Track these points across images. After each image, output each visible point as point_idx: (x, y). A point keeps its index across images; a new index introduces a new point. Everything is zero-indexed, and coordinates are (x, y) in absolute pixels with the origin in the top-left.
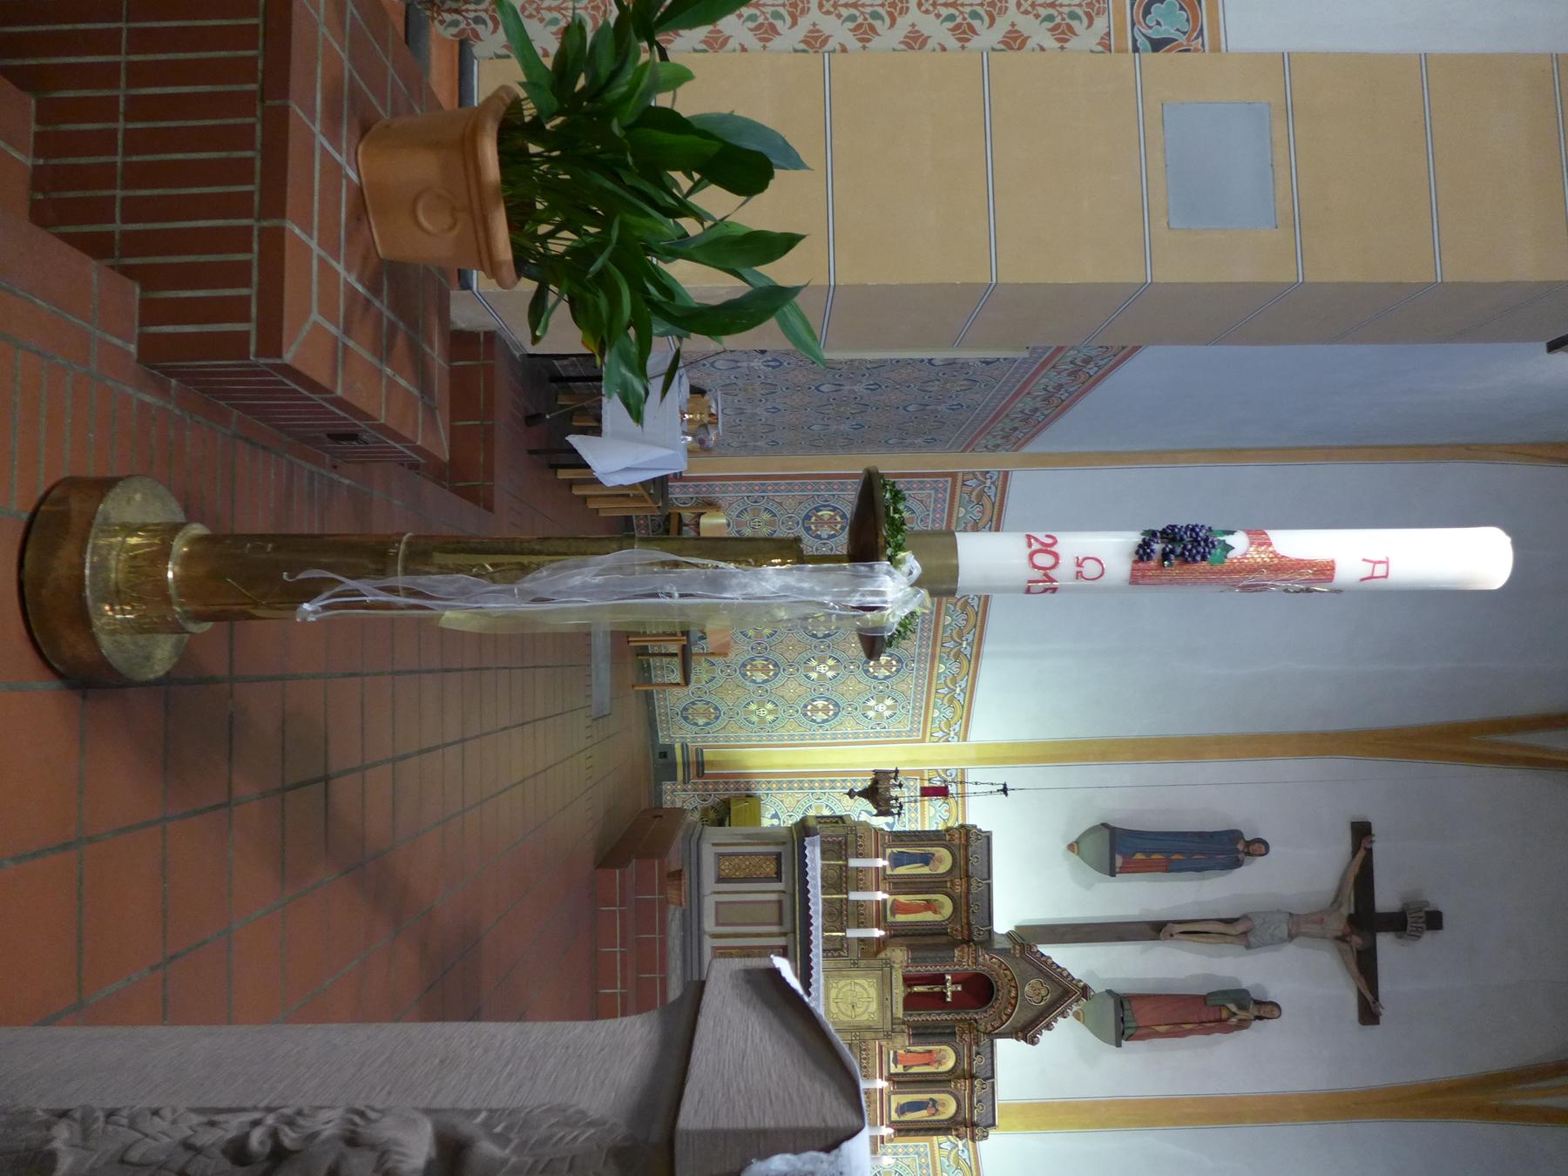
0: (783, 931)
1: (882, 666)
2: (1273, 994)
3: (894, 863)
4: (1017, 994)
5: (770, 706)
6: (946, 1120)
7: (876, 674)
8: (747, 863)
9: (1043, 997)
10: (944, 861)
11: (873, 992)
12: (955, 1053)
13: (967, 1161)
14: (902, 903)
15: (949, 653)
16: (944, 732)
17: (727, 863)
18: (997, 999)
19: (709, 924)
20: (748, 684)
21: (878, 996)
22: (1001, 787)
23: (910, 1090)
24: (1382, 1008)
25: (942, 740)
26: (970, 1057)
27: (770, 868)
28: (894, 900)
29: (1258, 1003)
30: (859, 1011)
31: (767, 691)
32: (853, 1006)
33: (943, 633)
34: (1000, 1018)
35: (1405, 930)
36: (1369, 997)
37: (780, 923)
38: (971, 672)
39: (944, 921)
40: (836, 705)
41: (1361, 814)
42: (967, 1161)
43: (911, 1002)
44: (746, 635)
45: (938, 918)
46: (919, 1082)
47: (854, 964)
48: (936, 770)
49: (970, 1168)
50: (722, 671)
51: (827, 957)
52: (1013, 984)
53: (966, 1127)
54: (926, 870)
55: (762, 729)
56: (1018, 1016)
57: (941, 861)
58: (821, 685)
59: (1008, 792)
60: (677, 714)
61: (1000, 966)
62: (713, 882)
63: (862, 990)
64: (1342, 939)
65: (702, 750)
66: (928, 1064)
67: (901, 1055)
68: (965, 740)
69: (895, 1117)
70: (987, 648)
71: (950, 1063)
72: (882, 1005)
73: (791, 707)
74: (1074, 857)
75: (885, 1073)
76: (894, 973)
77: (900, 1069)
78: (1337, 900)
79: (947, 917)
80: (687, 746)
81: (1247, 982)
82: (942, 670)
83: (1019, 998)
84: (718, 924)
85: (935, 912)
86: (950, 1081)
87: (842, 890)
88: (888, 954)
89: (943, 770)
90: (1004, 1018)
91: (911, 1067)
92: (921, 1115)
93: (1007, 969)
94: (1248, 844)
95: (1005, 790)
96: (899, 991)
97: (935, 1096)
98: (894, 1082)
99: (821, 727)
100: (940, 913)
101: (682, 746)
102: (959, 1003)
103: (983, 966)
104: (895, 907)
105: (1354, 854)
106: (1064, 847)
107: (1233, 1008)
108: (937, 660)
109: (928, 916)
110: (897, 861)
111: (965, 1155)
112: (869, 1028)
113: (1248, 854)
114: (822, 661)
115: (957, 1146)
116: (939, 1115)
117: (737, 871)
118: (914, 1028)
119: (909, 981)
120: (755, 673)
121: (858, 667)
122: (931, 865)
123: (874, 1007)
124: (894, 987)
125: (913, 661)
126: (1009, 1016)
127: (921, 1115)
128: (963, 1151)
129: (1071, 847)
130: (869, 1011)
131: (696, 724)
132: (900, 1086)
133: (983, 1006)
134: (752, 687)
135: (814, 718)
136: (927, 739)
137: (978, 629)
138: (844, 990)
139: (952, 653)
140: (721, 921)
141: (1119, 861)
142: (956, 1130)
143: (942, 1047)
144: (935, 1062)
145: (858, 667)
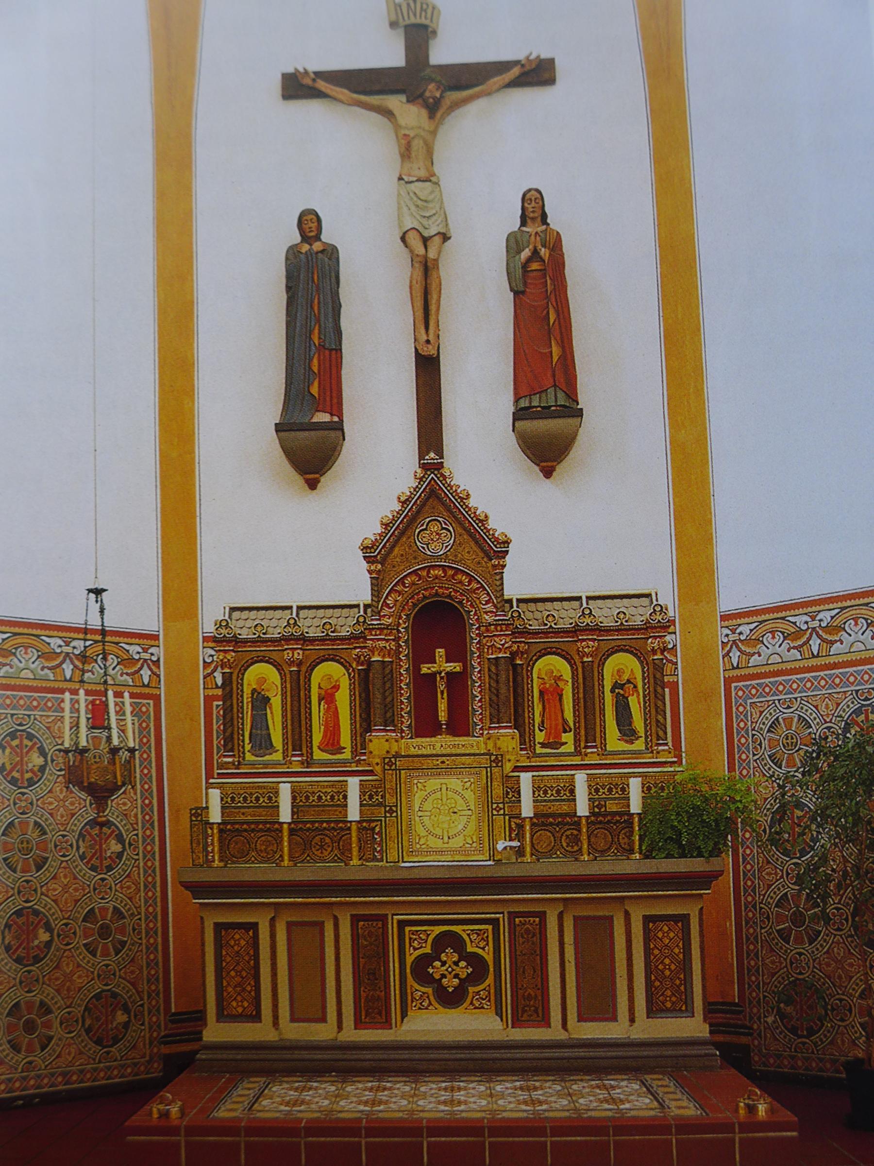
8: (233, 973)
9: (443, 529)
11: (433, 783)
12: (540, 657)
13: (752, 626)
14: (325, 736)
16: (142, 666)
17: (234, 1004)
19: (324, 1032)
22: (92, 596)
24: (531, 54)
27: (240, 939)
28: (319, 748)
30: (461, 805)
35: (425, 27)
39: (349, 674)
42: (752, 626)
45: (345, 683)
48: (205, 678)
52: (424, 573)
54: (276, 702)
56: (469, 554)
57: (262, 681)
60: (108, 1053)
61: (400, 593)
62: (259, 1024)
63: (430, 800)
65: (174, 1014)
66: (561, 696)
67: (548, 735)
68: (156, 637)
69: (639, 745)
72: (449, 771)
75: (577, 761)
76: (413, 751)
79: (343, 670)
80: (165, 1036)
84: (323, 1020)
85: (336, 688)
87: (277, 829)
88: (378, 760)
89: (205, 668)
90: (475, 585)
91: (565, 721)
92: (635, 704)
94: (305, 238)
96: (441, 743)
97: (608, 685)
99: (130, 844)
101: (166, 1043)
102: (458, 653)
109: (343, 699)
112: (487, 789)
113: (318, 238)
115: (734, 641)
117: (244, 990)
122: (268, 694)
123: (454, 783)
126: (471, 579)
128: (740, 633)
136: (155, 692)
140: (320, 1015)
143: (535, 676)
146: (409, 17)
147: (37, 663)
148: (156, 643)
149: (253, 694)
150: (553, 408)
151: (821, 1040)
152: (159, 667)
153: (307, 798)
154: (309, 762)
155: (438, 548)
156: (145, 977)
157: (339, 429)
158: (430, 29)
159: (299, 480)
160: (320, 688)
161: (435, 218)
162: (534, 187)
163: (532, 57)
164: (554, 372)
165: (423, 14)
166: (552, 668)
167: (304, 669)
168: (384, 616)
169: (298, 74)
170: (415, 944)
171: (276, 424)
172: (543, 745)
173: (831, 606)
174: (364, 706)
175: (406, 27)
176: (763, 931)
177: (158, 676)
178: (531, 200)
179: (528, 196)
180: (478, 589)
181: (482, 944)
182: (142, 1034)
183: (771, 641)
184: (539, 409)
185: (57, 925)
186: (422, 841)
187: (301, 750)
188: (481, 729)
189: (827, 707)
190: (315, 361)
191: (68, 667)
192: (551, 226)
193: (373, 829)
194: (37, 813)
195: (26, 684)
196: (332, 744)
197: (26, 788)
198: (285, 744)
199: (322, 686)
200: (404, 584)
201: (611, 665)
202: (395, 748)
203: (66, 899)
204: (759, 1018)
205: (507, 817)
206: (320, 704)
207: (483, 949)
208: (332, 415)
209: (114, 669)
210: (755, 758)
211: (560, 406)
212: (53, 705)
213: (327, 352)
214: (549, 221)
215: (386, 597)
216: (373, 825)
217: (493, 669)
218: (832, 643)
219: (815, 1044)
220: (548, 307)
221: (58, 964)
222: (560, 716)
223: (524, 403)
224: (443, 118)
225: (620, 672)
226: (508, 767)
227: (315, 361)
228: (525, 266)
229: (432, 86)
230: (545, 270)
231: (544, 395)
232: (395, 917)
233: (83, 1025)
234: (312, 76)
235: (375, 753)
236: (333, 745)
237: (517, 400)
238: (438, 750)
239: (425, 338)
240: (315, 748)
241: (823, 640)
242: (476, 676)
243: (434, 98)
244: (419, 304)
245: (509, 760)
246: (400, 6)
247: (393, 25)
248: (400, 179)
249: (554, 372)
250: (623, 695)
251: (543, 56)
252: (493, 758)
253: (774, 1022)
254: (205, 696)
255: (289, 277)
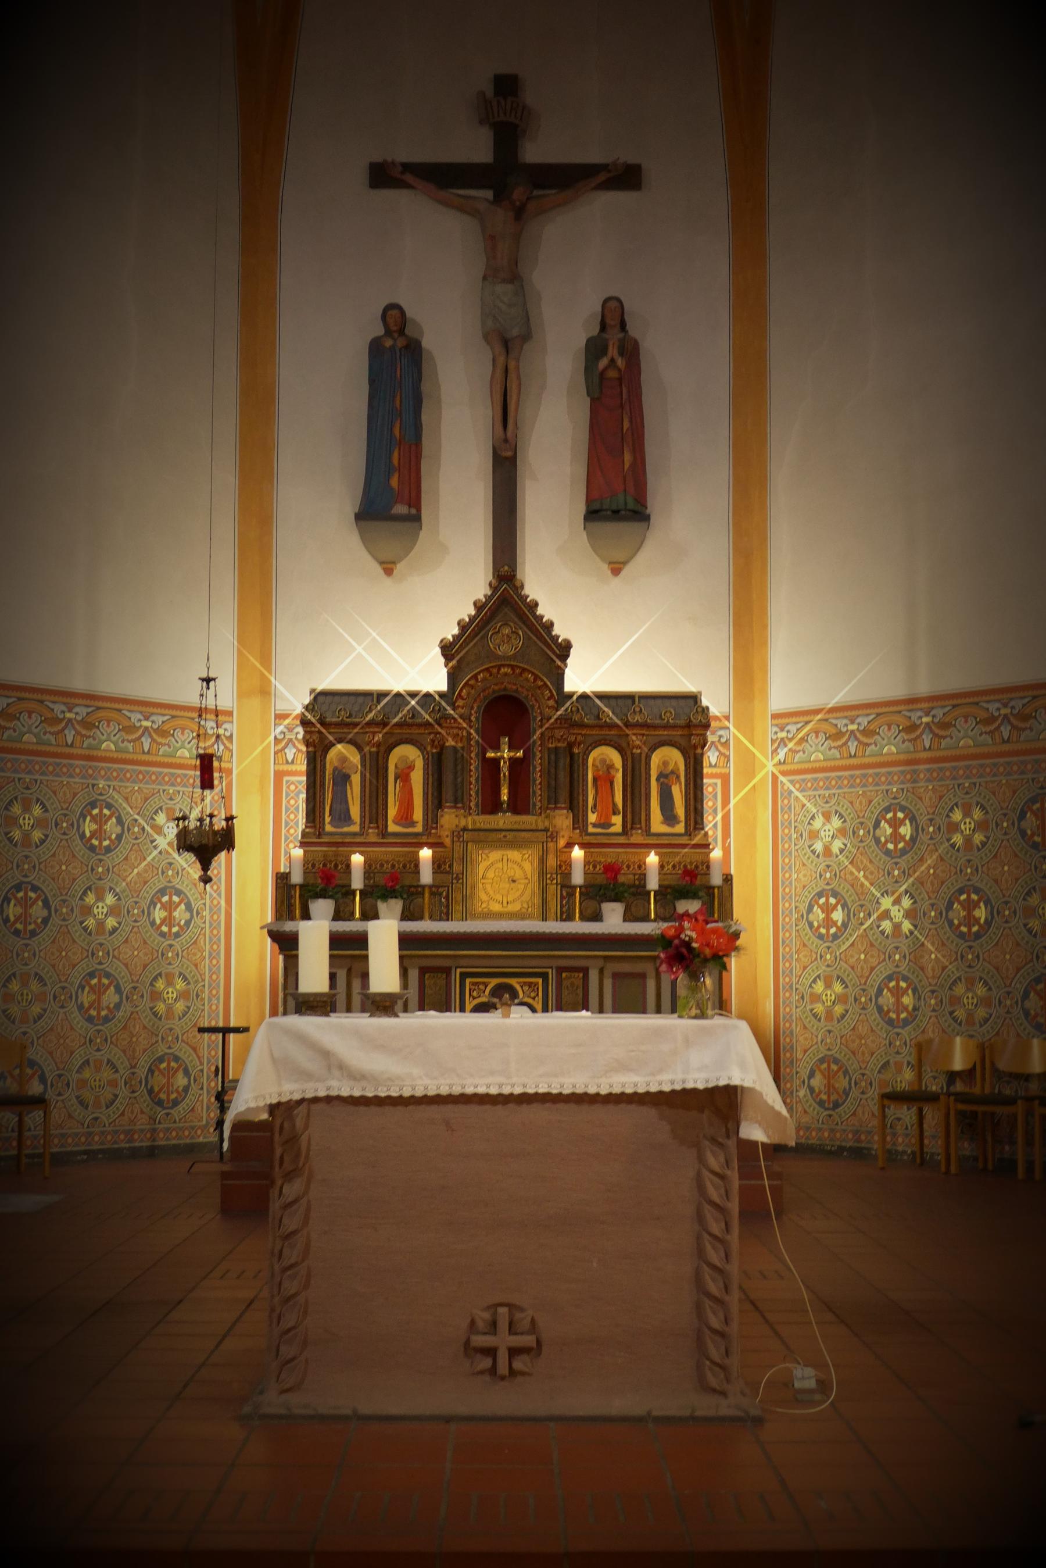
0: (654, 974)
1: (101, 827)
2: (595, 306)
3: (345, 821)
4: (509, 666)
5: (160, 985)
6: (685, 761)
7: (114, 836)
10: (342, 753)
11: (495, 855)
15: (83, 736)
18: (517, 691)
20: (121, 1014)
21: (497, 848)
23: (643, 805)
25: (228, 744)
26: (601, 727)
28: (394, 821)
29: (603, 327)
30: (518, 874)
31: (135, 988)
32: (514, 881)
33: (51, 745)
34: (539, 688)
36: (602, 177)
37: (643, 976)
38: (117, 706)
40: (162, 892)
41: (360, 175)
43: (519, 805)
44: (40, 1016)
45: (419, 764)
46: (633, 794)
47: (457, 878)
48: (275, 753)
49: (1034, 697)
50: (98, 1050)
51: (447, 914)
52: (495, 671)
53: (692, 734)
54: (356, 779)
55: (197, 996)
58: (128, 912)
59: (211, 675)
60: (168, 1114)
61: (472, 687)
64: (519, 213)
66: (612, 783)
67: (600, 817)
69: (680, 828)
70: (79, 684)
71: (614, 757)
72: (513, 845)
73: (163, 954)
74: (400, 568)
75: (622, 840)
77: (617, 820)
78: (473, 213)
79: (418, 753)
81: (579, 340)
82: (113, 747)
83: (512, 663)
85: (411, 768)
86: (632, 754)
89: (275, 744)
91: (614, 805)
92: (678, 793)
93: (475, 677)
94: (388, 332)
95: (208, 680)
96: (504, 820)
98: (632, 828)
99: (198, 913)
100: (414, 761)
103: (472, 708)
104: (404, 821)
105: (408, 186)
106: (387, 581)
107: (603, 363)
108: (95, 753)
109: (417, 778)
110: (342, 816)
111: (793, 728)
112: (543, 861)
113: (401, 332)
114: (88, 911)
115: (1005, 716)
116: (678, 769)
118: (549, 803)
119: (492, 806)
120: (104, 1004)
121: (101, 861)
122: (348, 771)
123: (514, 855)
124: (496, 827)
125: (93, 785)
127: (678, 793)
128: (788, 732)
129: (389, 572)
130: (519, 860)
131: (186, 1089)
132: (637, 819)
133: (527, 710)
134: (127, 1008)
135: (182, 923)
137: (44, 697)
138: (491, 893)
139: (84, 732)
141: (401, 509)
142: (695, 747)
144: (609, 773)
145: (101, 861)
146: (498, 116)
147: (117, 736)
148: (230, 719)
149: (334, 771)
151: (845, 1112)
152: (232, 742)
153: (382, 865)
154: (384, 833)
155: (505, 650)
156: (206, 1042)
159: (378, 570)
160: (396, 767)
162: (616, 294)
163: (621, 161)
166: (605, 757)
167: (382, 749)
168: (458, 706)
170: (475, 994)
172: (594, 825)
173: (868, 711)
174: (435, 784)
176: (798, 1010)
177: (231, 751)
180: (542, 686)
181: (533, 995)
182: (201, 1098)
183: (815, 740)
185: (126, 988)
186: (484, 905)
187: (377, 823)
188: (540, 808)
189: (861, 803)
190: (396, 454)
191: (70, 733)
192: (630, 333)
193: (441, 894)
194: (113, 880)
195: (35, 748)
196: (406, 818)
197: (104, 855)
198: (363, 817)
199: (399, 766)
200: (477, 680)
201: (656, 759)
202: (463, 823)
203: (136, 964)
204: (792, 1093)
205: (559, 887)
206: (396, 783)
207: (534, 999)
208: (410, 507)
209: (189, 743)
210: (797, 847)
211: (630, 510)
212: (131, 776)
215: (461, 690)
216: (441, 890)
217: (553, 757)
218: (868, 745)
219: (840, 1116)
221: (125, 1025)
222: (610, 799)
225: (665, 763)
226: (562, 843)
227: (396, 454)
232: (458, 970)
233: (146, 1085)
235: (446, 826)
236: (406, 818)
238: (501, 825)
240: (390, 822)
241: (860, 742)
242: (537, 761)
244: (498, 398)
245: (563, 837)
247: (486, 337)
250: (667, 785)
251: (629, 162)
252: (549, 834)
253: (805, 1096)
254: (275, 772)
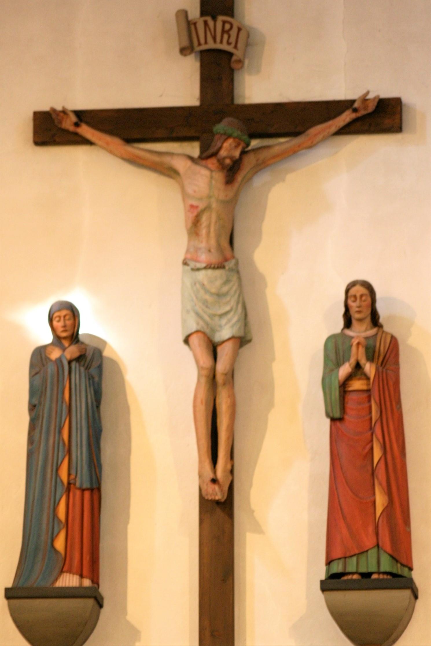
24: (368, 93)
150: (375, 576)
157: (407, 588)
158: (234, 58)
161: (230, 316)
164: (377, 527)
165: (226, 37)
169: (54, 116)
171: (7, 590)
175: (202, 52)
178: (355, 296)
179: (352, 292)
184: (355, 577)
208: (81, 576)
213: (78, 493)
214: (381, 320)
220: (372, 441)
223: (337, 568)
224: (248, 180)
228: (344, 385)
229: (228, 144)
230: (368, 391)
231: (363, 558)
234: (73, 118)
237: (329, 563)
239: (211, 476)
243: (231, 158)
246: (195, 24)
248: (185, 263)
249: (377, 527)
255: (32, 392)
